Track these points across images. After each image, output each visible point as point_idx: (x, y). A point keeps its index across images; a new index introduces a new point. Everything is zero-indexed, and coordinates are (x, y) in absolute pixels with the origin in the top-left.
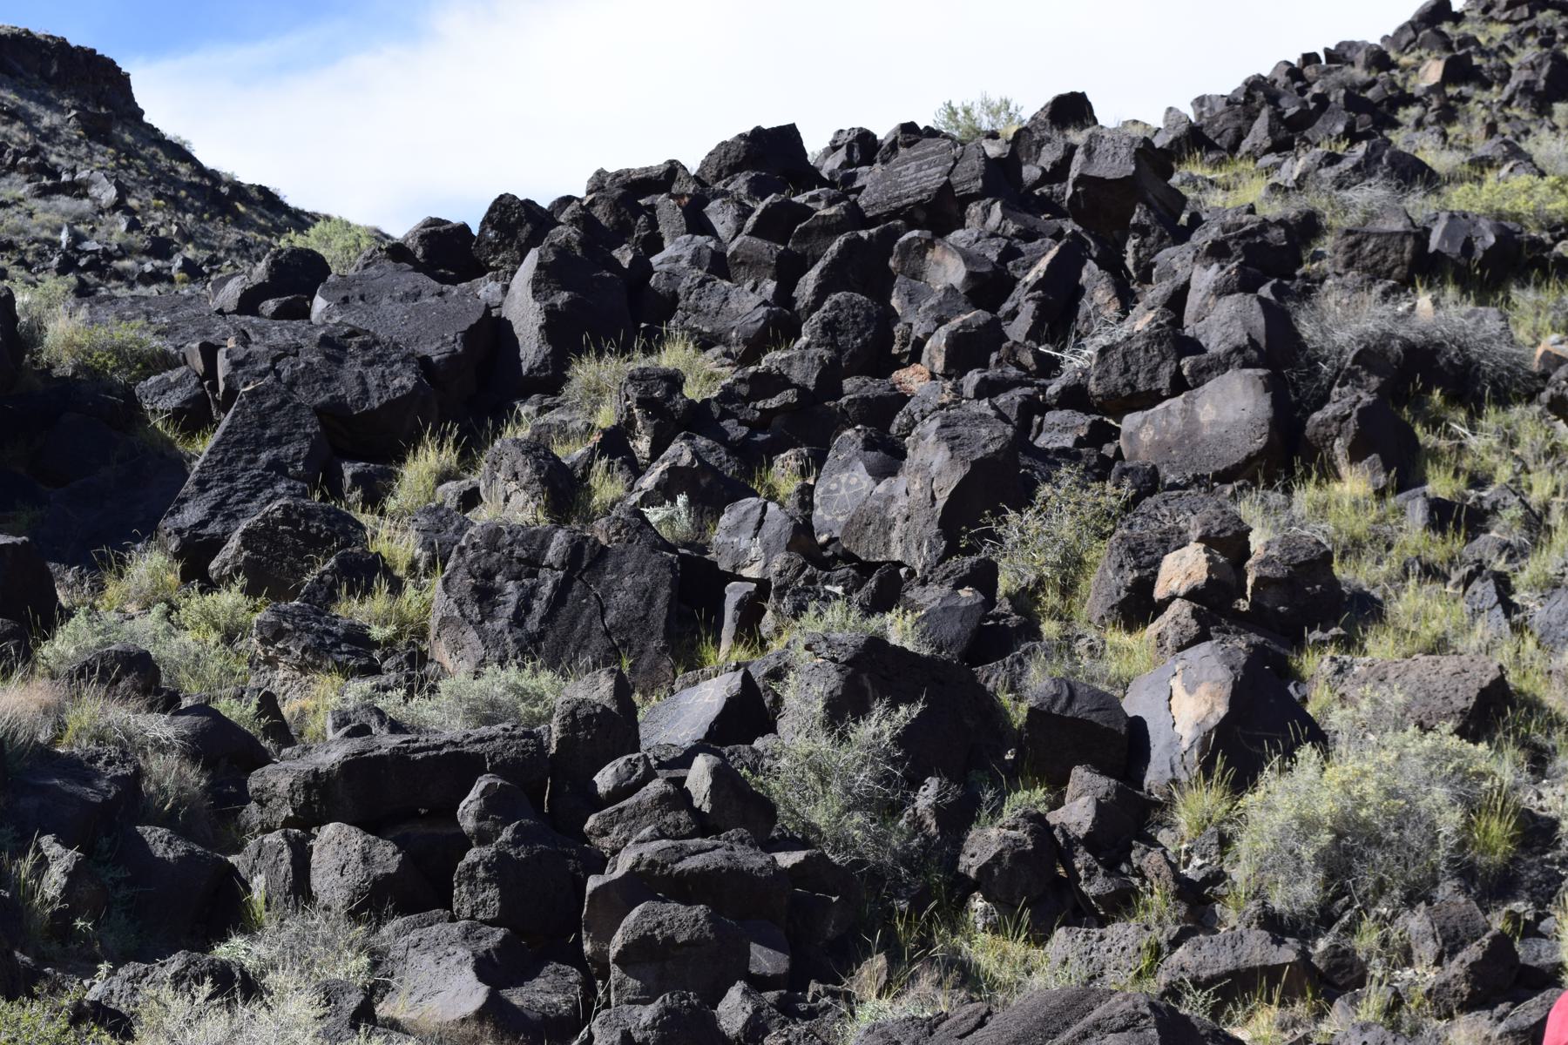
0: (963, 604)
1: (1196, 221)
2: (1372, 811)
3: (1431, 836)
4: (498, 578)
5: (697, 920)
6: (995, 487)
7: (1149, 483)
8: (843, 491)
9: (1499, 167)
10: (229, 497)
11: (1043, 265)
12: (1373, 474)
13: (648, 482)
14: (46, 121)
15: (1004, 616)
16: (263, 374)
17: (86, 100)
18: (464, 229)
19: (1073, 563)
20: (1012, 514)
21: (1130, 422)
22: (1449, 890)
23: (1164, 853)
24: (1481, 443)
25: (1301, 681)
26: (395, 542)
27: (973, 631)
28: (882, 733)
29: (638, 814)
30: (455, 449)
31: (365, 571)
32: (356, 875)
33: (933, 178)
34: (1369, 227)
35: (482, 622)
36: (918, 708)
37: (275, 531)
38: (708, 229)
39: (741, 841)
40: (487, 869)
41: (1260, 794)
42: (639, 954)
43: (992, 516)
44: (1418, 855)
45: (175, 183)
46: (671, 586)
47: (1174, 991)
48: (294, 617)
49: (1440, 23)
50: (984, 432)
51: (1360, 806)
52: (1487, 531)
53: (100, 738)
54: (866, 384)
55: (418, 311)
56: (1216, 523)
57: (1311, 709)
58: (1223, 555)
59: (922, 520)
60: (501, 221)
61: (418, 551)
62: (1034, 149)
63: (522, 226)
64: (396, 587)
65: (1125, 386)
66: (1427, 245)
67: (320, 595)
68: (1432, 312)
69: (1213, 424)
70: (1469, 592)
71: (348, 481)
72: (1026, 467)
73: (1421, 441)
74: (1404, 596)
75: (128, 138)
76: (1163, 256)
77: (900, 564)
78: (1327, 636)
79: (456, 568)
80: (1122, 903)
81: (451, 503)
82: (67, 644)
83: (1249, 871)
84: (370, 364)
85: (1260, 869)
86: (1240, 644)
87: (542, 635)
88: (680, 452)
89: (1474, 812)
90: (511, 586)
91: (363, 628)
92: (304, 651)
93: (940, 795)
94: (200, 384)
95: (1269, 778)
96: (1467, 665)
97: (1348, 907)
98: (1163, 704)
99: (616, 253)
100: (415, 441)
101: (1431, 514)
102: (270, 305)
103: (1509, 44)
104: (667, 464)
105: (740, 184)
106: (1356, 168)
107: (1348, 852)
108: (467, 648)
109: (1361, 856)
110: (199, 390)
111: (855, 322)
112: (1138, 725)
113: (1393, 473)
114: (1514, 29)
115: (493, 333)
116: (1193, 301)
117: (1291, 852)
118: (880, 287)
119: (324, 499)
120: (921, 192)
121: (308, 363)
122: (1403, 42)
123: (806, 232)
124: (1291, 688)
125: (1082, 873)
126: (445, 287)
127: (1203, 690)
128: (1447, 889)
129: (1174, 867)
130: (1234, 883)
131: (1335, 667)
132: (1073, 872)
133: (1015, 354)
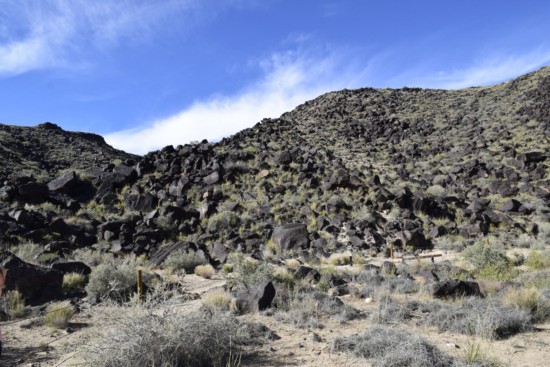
6: (187, 187)
19: (195, 195)
21: (204, 178)
24: (242, 178)
26: (121, 197)
29: (141, 227)
31: (117, 201)
32: (109, 236)
33: (186, 151)
42: (139, 242)
45: (110, 151)
47: (200, 241)
53: (80, 223)
64: (121, 203)
68: (238, 163)
80: (196, 231)
82: (80, 212)
88: (155, 185)
100: (124, 186)
105: (165, 153)
112: (199, 212)
115: (135, 172)
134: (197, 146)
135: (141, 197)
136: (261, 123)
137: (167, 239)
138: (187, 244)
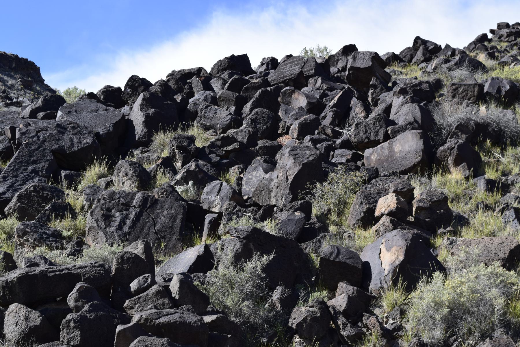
0: (296, 218)
1: (395, 84)
2: (465, 299)
3: (491, 309)
4: (113, 211)
5: (163, 345)
6: (312, 173)
7: (375, 174)
8: (254, 179)
9: (510, 65)
10: (15, 183)
11: (336, 99)
12: (464, 171)
13: (178, 177)
14: (10, 82)
15: (314, 223)
16: (32, 137)
17: (24, 76)
18: (119, 89)
19: (342, 205)
20: (318, 185)
21: (368, 152)
22: (499, 333)
23: (377, 318)
25: (435, 248)
26: (76, 198)
27: (300, 229)
28: (257, 266)
29: (147, 300)
30: (106, 166)
31: (63, 210)
32: (21, 327)
34: (461, 83)
35: (105, 228)
36: (271, 257)
37: (30, 195)
38: (211, 89)
39: (188, 310)
40: (75, 322)
41: (418, 292)
43: (310, 184)
44: (486, 318)
46: (183, 214)
48: (31, 227)
49: (484, 42)
50: (308, 152)
51: (461, 297)
52: (510, 192)
54: (267, 142)
55: (97, 116)
56: (400, 185)
57: (440, 259)
58: (403, 198)
59: (283, 188)
60: (132, 85)
61: (85, 202)
62: (335, 63)
63: (140, 87)
64: (74, 216)
65: (366, 138)
66: (483, 89)
67: (44, 219)
69: (400, 152)
70: (504, 214)
71: (63, 178)
72: (325, 168)
73: (483, 159)
74: (477, 217)
75: (38, 88)
76: (382, 96)
77: (275, 206)
78: (446, 231)
79: (96, 207)
81: (103, 186)
83: (413, 325)
84: (76, 134)
85: (418, 324)
86: (410, 233)
87: (129, 233)
88: (192, 166)
89: (509, 300)
90: (118, 214)
91: (60, 231)
92: (35, 240)
93: (282, 294)
94: (10, 142)
95: (421, 285)
96: (504, 240)
97: (456, 340)
98: (377, 256)
99: (175, 97)
100: (90, 163)
101: (487, 185)
102: (41, 115)
103: (508, 49)
104: (186, 170)
105: (225, 75)
106: (456, 64)
107: (455, 316)
108: (99, 238)
109: (461, 319)
110: (9, 144)
111: (264, 120)
112: (367, 265)
113: (472, 170)
114: (510, 44)
115: (126, 124)
116: (393, 110)
117: (431, 317)
118: (274, 107)
119: (52, 184)
120: (291, 75)
121: (50, 134)
122: (471, 49)
124: (431, 251)
125: (341, 326)
126: (108, 108)
127: (393, 249)
128: (498, 333)
129: (381, 324)
130: (407, 331)
131: (449, 242)
132: (338, 326)
133: (324, 130)
134: (331, 60)
136: (490, 36)
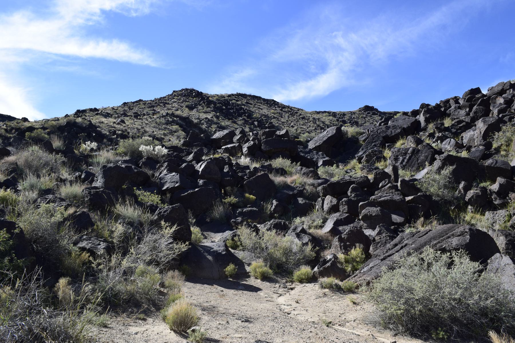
32: (329, 205)
36: (455, 166)
40: (345, 202)
87: (406, 165)
102: (383, 124)
115: (418, 123)
123: (475, 100)
135: (414, 150)
137: (427, 217)
138: (462, 234)
